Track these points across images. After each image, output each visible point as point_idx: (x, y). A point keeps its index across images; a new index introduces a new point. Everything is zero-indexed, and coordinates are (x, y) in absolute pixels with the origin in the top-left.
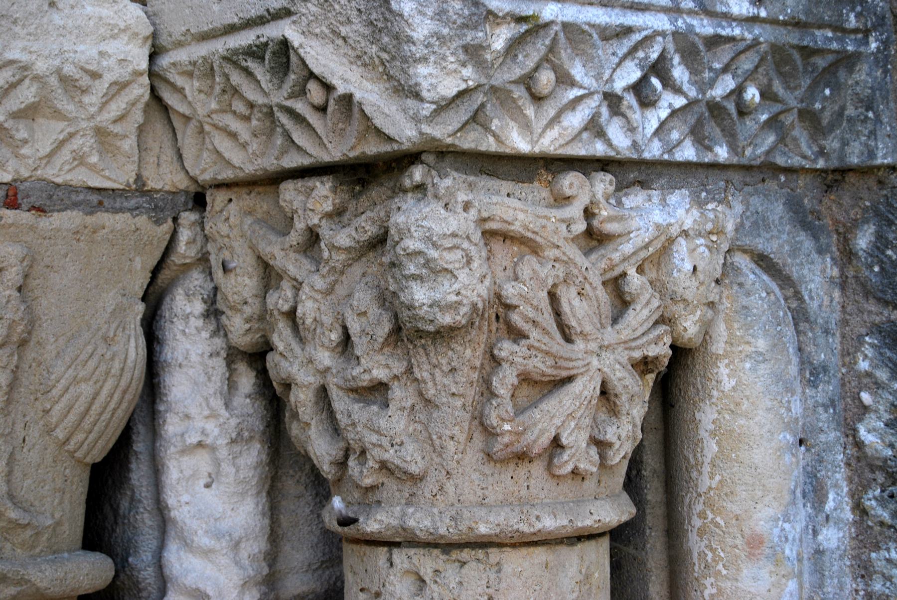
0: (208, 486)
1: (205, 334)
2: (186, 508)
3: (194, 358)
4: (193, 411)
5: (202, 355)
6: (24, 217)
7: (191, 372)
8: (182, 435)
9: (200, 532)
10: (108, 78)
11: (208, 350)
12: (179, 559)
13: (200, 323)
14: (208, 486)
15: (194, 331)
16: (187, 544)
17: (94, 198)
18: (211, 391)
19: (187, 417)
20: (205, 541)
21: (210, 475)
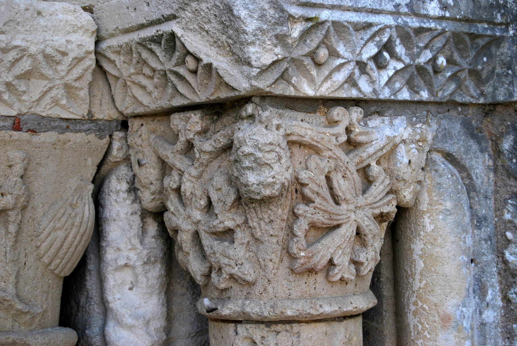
0: (131, 289)
1: (128, 202)
2: (118, 302)
3: (122, 215)
4: (122, 246)
5: (127, 214)
6: (24, 135)
7: (120, 223)
8: (116, 260)
9: (127, 316)
10: (72, 55)
11: (130, 211)
12: (115, 331)
13: (125, 195)
14: (131, 289)
15: (122, 200)
16: (119, 323)
17: (64, 124)
18: (132, 234)
19: (119, 249)
20: (129, 321)
21: (132, 283)
